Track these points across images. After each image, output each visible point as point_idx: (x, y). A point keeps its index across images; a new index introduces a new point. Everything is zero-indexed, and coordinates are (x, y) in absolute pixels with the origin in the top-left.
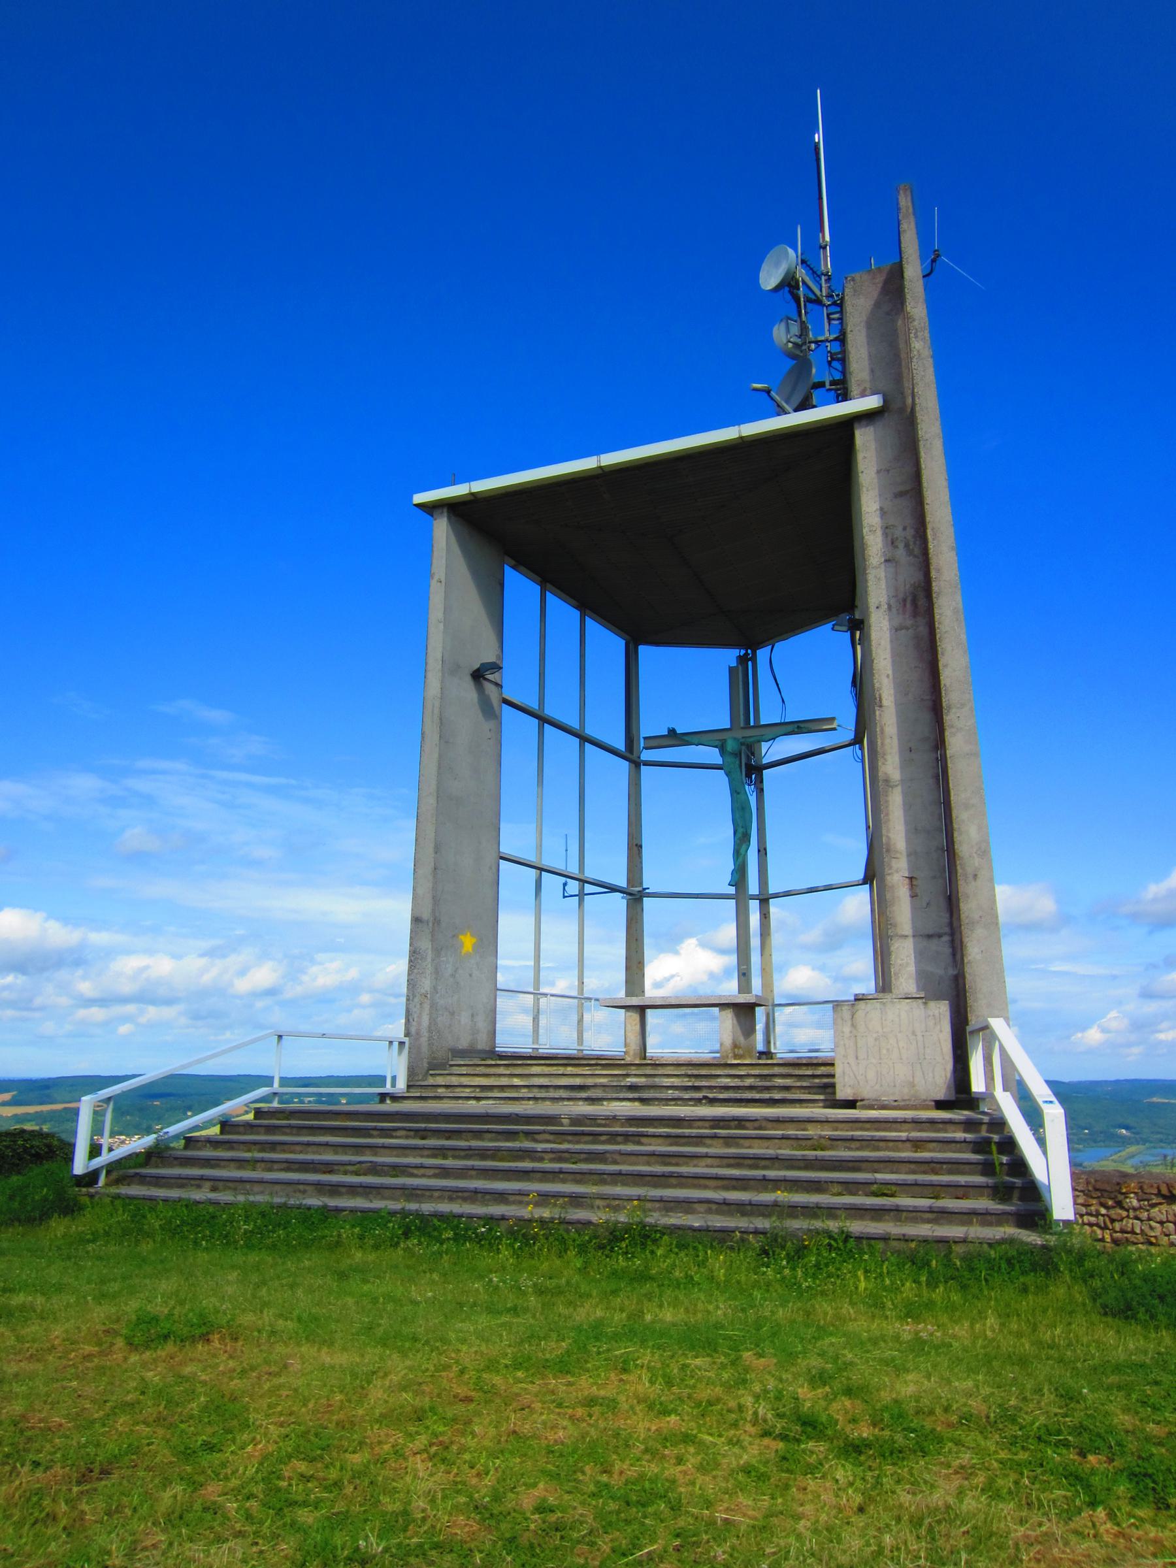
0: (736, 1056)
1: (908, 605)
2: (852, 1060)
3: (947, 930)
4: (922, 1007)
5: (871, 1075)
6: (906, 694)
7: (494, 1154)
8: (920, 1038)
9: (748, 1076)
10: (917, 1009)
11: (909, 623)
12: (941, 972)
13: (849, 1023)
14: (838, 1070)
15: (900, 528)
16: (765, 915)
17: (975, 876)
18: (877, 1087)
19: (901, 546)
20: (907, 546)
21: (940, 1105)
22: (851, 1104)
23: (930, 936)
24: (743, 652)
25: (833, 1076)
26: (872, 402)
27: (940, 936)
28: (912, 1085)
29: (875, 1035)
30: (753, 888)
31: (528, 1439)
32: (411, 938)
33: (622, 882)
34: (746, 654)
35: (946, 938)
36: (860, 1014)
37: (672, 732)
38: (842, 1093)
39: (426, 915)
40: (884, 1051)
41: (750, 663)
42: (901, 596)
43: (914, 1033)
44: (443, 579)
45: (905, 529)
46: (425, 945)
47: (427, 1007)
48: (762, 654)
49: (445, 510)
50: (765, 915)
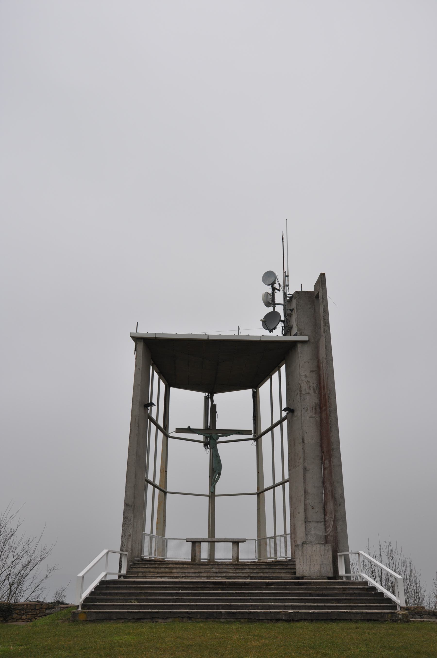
1: (314, 410)
2: (302, 564)
3: (323, 520)
5: (308, 569)
6: (312, 440)
7: (199, 594)
8: (323, 556)
9: (257, 568)
10: (322, 547)
11: (314, 416)
12: (321, 534)
15: (312, 383)
17: (340, 505)
19: (312, 389)
20: (314, 389)
21: (329, 578)
22: (302, 578)
23: (318, 522)
24: (207, 394)
25: (295, 569)
26: (306, 338)
27: (321, 522)
28: (320, 572)
32: (124, 512)
35: (323, 523)
38: (297, 575)
39: (131, 504)
41: (210, 399)
42: (311, 406)
43: (321, 555)
44: (141, 368)
45: (313, 383)
46: (130, 515)
47: (130, 540)
49: (142, 341)
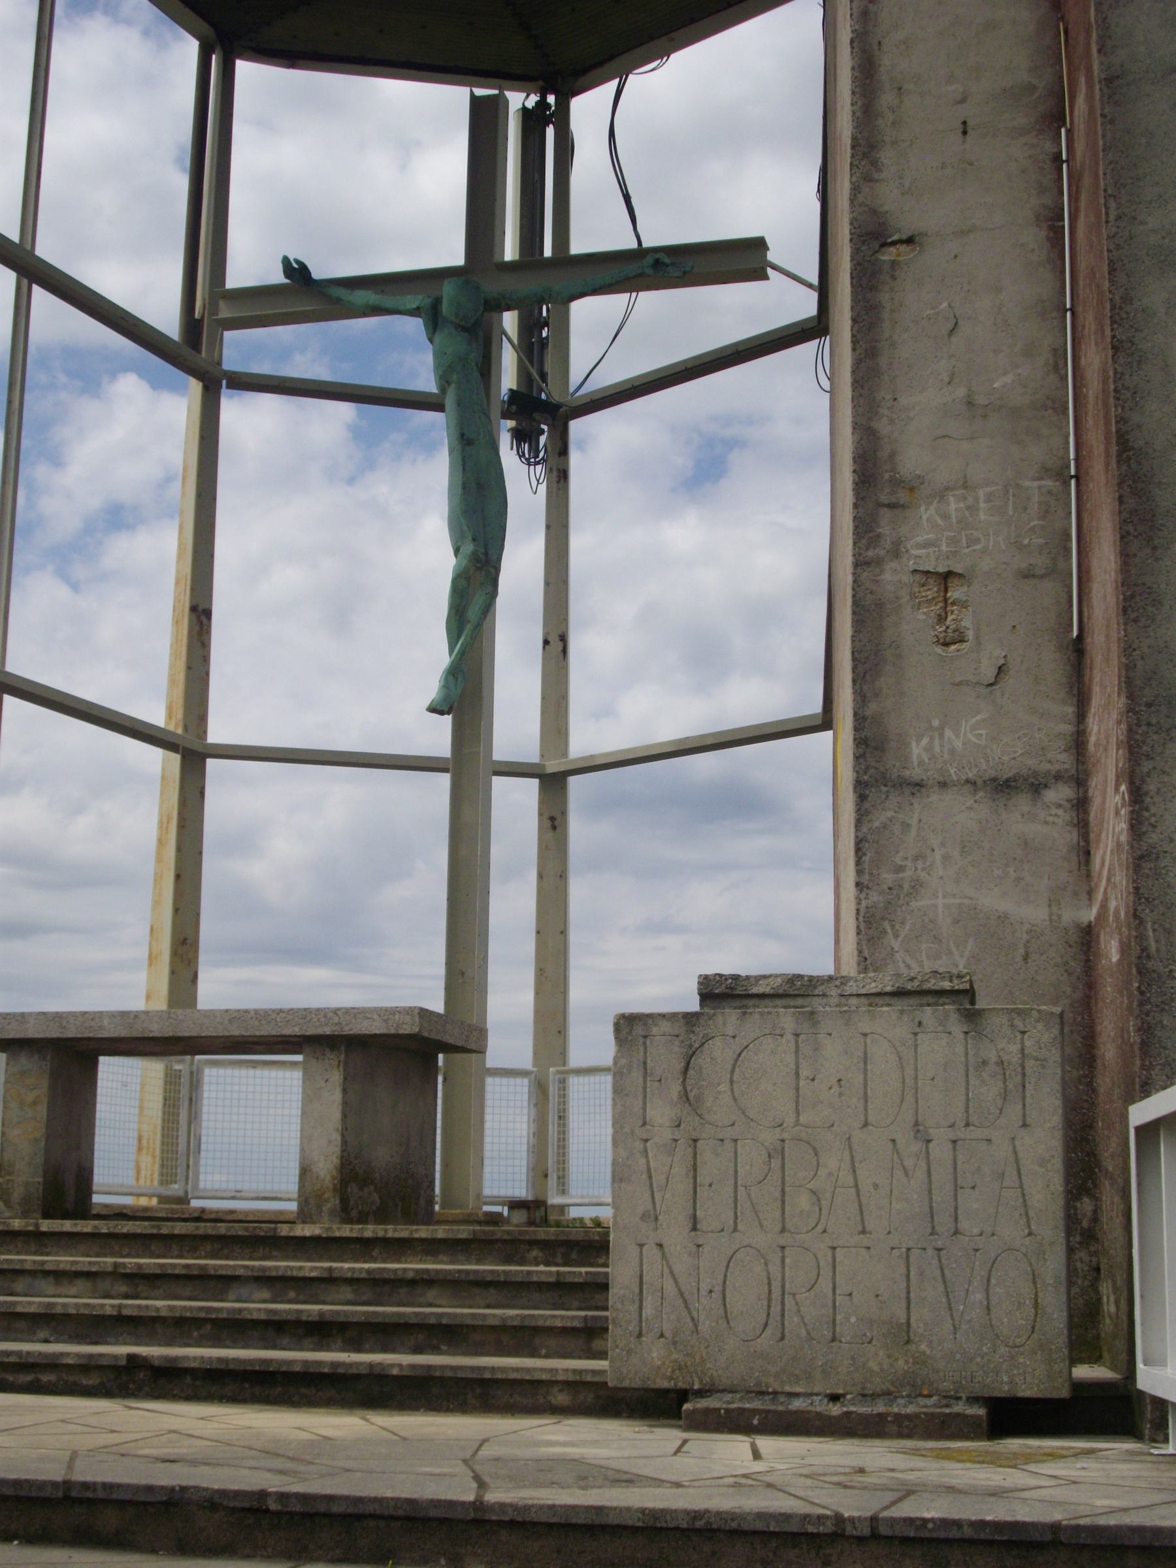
0: (346, 1213)
2: (676, 1235)
3: (1063, 760)
4: (957, 1027)
5: (746, 1295)
8: (940, 1151)
13: (675, 1088)
14: (620, 1271)
16: (554, 821)
18: (766, 1341)
28: (903, 1334)
29: (769, 1137)
30: (515, 725)
31: (1144, 949)
33: (155, 714)
34: (542, 104)
35: (1060, 793)
36: (719, 1052)
37: (297, 272)
40: (804, 1201)
41: (550, 131)
48: (588, 110)
50: (554, 821)
